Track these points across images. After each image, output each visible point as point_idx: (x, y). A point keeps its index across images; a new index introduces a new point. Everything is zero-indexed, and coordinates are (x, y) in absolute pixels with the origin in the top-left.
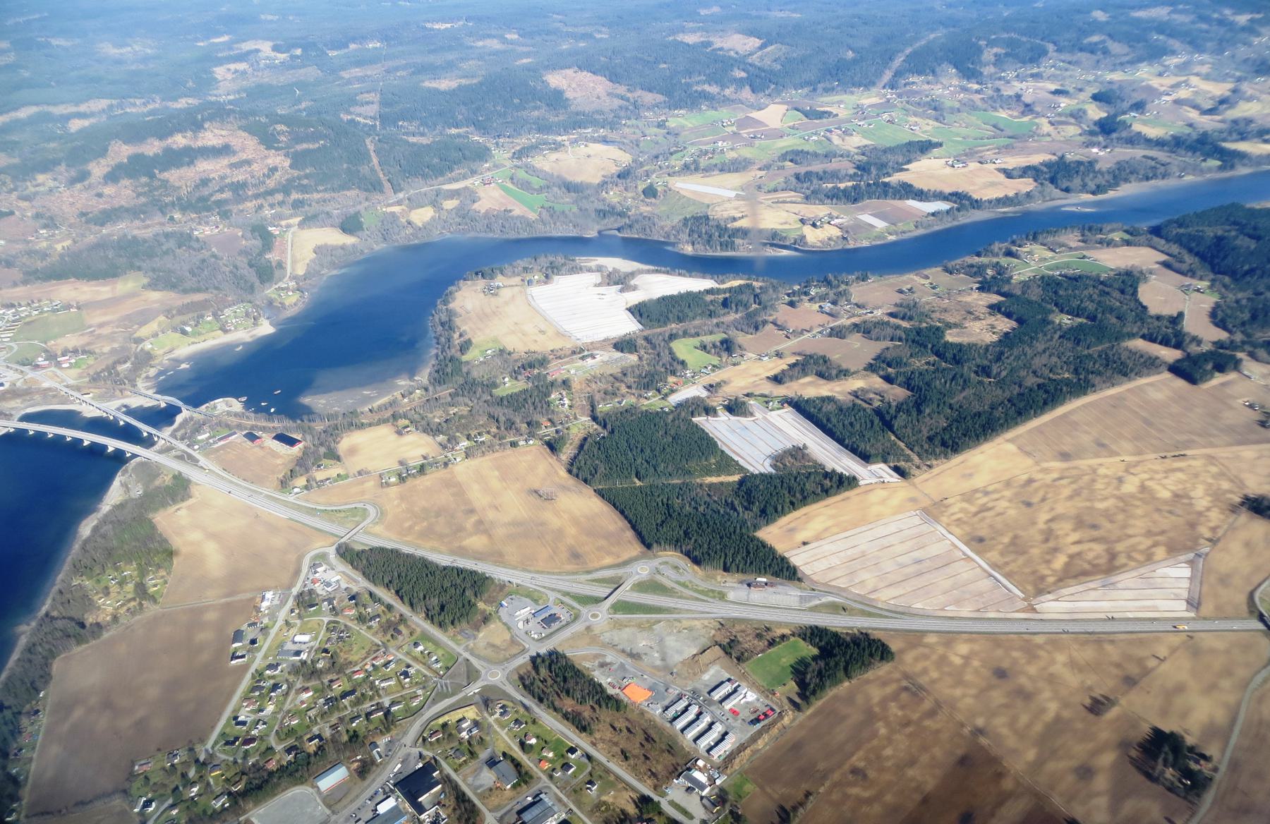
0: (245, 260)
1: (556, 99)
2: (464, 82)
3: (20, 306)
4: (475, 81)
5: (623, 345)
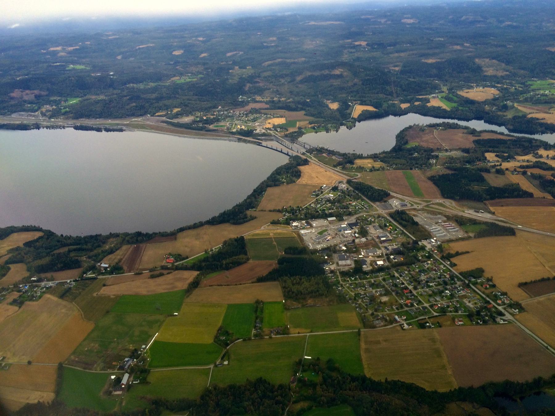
0: (410, 168)
1: (479, 69)
2: (438, 60)
3: (268, 114)
4: (443, 60)
5: (466, 151)
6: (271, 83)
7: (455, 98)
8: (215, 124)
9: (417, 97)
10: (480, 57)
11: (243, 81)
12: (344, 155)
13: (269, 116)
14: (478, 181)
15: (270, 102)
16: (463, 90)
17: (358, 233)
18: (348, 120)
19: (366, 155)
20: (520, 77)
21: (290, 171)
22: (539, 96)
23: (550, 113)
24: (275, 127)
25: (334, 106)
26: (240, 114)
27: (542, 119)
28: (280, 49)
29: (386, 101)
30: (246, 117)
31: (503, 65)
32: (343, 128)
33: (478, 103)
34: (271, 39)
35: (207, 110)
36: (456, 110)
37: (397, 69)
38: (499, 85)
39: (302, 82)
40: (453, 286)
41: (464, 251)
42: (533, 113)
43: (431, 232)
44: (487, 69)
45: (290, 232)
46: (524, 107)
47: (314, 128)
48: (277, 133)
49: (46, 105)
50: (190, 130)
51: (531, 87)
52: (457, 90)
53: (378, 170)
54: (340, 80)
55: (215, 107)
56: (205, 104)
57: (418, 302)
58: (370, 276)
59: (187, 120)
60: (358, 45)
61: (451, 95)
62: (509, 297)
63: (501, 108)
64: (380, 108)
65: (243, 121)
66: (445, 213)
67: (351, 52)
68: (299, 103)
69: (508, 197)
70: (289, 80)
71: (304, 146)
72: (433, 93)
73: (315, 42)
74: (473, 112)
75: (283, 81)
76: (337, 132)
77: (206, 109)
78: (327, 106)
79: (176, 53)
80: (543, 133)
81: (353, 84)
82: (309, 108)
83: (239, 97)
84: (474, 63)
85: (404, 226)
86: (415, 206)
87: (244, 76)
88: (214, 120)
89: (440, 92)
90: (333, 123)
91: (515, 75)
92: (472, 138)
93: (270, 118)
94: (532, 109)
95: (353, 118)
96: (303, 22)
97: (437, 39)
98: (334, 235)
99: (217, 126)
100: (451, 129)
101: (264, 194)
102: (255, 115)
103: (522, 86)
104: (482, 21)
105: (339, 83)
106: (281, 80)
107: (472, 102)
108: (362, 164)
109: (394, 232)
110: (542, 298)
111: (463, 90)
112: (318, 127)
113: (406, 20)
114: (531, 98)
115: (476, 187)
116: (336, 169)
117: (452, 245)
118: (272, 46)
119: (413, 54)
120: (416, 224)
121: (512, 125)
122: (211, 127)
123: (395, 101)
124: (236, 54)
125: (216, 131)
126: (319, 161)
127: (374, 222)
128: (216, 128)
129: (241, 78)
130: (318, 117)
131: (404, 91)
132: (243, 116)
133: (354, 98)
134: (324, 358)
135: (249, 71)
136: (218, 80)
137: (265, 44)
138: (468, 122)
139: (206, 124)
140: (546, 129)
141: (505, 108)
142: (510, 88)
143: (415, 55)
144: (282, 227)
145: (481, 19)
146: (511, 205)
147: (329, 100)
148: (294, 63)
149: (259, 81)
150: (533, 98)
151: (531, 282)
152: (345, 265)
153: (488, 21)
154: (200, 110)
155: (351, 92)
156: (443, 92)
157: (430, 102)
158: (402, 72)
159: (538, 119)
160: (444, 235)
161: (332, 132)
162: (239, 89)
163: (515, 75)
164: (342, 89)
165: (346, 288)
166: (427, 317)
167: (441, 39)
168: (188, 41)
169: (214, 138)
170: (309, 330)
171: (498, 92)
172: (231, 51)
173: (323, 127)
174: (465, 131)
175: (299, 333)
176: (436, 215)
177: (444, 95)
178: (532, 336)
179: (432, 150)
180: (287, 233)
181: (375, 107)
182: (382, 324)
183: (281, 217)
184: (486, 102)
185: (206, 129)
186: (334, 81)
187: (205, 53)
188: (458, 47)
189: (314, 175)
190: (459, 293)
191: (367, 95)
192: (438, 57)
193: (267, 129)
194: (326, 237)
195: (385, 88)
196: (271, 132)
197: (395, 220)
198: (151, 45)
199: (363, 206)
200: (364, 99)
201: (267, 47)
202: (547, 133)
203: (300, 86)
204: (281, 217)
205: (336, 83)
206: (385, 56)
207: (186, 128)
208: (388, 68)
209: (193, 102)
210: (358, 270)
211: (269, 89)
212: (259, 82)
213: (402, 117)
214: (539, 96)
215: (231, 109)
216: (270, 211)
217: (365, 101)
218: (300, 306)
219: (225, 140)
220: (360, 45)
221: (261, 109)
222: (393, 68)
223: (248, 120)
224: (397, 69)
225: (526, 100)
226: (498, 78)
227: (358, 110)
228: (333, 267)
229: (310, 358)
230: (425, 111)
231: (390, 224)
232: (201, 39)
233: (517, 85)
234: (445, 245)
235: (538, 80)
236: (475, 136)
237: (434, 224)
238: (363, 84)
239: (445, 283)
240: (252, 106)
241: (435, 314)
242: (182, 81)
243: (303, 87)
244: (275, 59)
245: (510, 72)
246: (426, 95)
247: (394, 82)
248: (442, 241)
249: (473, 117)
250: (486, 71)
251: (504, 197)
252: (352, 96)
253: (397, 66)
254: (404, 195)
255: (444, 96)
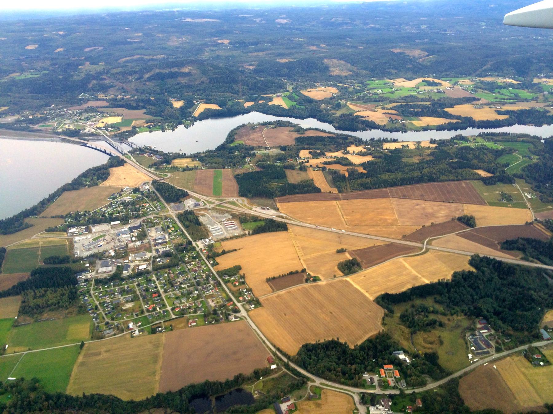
3: (105, 113)
6: (117, 80)
7: (297, 97)
8: (42, 124)
9: (262, 96)
10: (330, 58)
11: (89, 77)
12: (165, 154)
13: (105, 114)
14: (278, 178)
15: (113, 100)
16: (306, 89)
17: (135, 237)
18: (188, 119)
19: (189, 155)
20: (362, 76)
21: (96, 174)
22: (371, 95)
23: (375, 111)
24: (106, 127)
25: (178, 104)
26: (73, 113)
27: (366, 117)
28: (143, 45)
29: (232, 99)
30: (79, 116)
31: (349, 65)
32: (181, 127)
33: (316, 101)
34: (137, 34)
35: (38, 108)
36: (293, 109)
37: (251, 68)
38: (341, 85)
39: (150, 79)
40: (204, 286)
41: (232, 249)
42: (360, 111)
43: (210, 232)
44: (334, 69)
45: (63, 239)
46: (354, 105)
47: (149, 127)
48: (107, 132)
49: (84, 93)
50: (12, 131)
51: (368, 86)
52: (301, 89)
53: (191, 170)
54: (187, 78)
55: (48, 105)
56: (37, 103)
57: (161, 306)
58: (126, 282)
59: (10, 119)
60: (220, 43)
61: (294, 95)
62: (252, 293)
63: (335, 107)
64: (224, 107)
65: (74, 120)
66: (233, 211)
67: (213, 50)
68: (142, 101)
69: (298, 193)
70: (136, 77)
71: (132, 145)
72: (278, 92)
73: (181, 39)
74: (307, 110)
75: (130, 78)
76: (173, 131)
77: (36, 107)
78: (171, 104)
79: (30, 47)
80: (363, 129)
81: (200, 82)
82: (151, 107)
83: (81, 94)
84: (323, 64)
85: (186, 227)
86: (208, 206)
87: (92, 72)
88: (41, 120)
89: (285, 91)
90: (171, 122)
91: (357, 75)
92: (296, 135)
93: (106, 117)
94: (361, 107)
95: (193, 117)
96: (179, 19)
97: (297, 39)
98: (109, 240)
99: (43, 126)
100: (282, 128)
101: (57, 199)
102: (90, 114)
103: (361, 85)
104: (349, 23)
105: (187, 82)
106: (129, 77)
107: (310, 101)
108: (179, 163)
109: (174, 233)
110: (282, 292)
111: (306, 89)
112: (154, 126)
113: (280, 20)
114: (364, 97)
115: (274, 185)
116: (149, 170)
117: (223, 243)
118: (135, 42)
119: (270, 54)
120: (199, 224)
121: (337, 122)
122: (36, 127)
123: (241, 99)
124: (95, 49)
125: (40, 131)
126: (137, 161)
127: (158, 224)
128: (40, 128)
129: (87, 75)
130: (156, 116)
131: (250, 89)
132: (76, 115)
133: (200, 97)
134: (29, 378)
135: (101, 66)
136: (61, 77)
137: (129, 40)
138: (303, 120)
139: (30, 123)
140: (366, 126)
141: (339, 106)
142: (349, 88)
143: (272, 54)
144: (57, 234)
145: (349, 21)
146: (299, 200)
147: (174, 98)
148: (152, 60)
149: (106, 77)
150: (365, 97)
151: (280, 277)
152: (105, 272)
153: (355, 23)
154: (30, 108)
155: (198, 90)
156: (288, 91)
157: (272, 101)
158: (256, 71)
159: (362, 117)
160: (221, 234)
161: (168, 131)
162: (82, 86)
163: (357, 75)
164: (189, 87)
165: (94, 298)
166: (162, 321)
167: (301, 39)
168: (45, 35)
169: (36, 138)
170: (27, 349)
171: (337, 91)
172: (90, 46)
173: (159, 126)
174: (293, 129)
175: (15, 352)
176: (224, 213)
177: (288, 93)
178: (256, 331)
179: (252, 148)
180: (59, 241)
181: (220, 106)
182: (113, 333)
183: (60, 223)
184: (321, 102)
185: (29, 129)
186: (183, 79)
187: (61, 48)
188: (314, 48)
189: (122, 177)
190: (208, 292)
191: (213, 94)
192: (293, 57)
193: (98, 128)
194: (98, 243)
195: (232, 86)
196: (101, 132)
197: (181, 221)
198: (3, 39)
199: (156, 207)
200: (210, 97)
201: (130, 43)
202: (367, 130)
203: (147, 83)
204: (60, 223)
205: (183, 81)
206: (244, 55)
207: (7, 128)
208: (243, 67)
209: (25, 100)
210: (116, 278)
211: (115, 86)
212: (105, 80)
213: (245, 115)
214: (371, 95)
215: (66, 107)
216: (53, 217)
217: (210, 100)
218: (32, 321)
219: (48, 141)
220: (223, 43)
221: (97, 107)
222: (248, 67)
223: (80, 119)
224: (251, 68)
225: (359, 99)
226: (341, 78)
227: (202, 107)
228: (90, 275)
229: (14, 379)
230: (266, 110)
231: (174, 225)
232: (61, 33)
233: (356, 85)
234: (217, 245)
235: (376, 80)
236: (299, 134)
237: (217, 223)
238: (210, 82)
239: (198, 283)
240: (92, 104)
241: (174, 317)
242: (23, 77)
243: (150, 85)
244: (133, 56)
245: (354, 72)
246: (271, 93)
247: (242, 81)
248: (216, 240)
249: (308, 115)
250: (332, 71)
251: (295, 193)
252: (198, 95)
253: (251, 65)
254: (202, 195)
255: (288, 95)
